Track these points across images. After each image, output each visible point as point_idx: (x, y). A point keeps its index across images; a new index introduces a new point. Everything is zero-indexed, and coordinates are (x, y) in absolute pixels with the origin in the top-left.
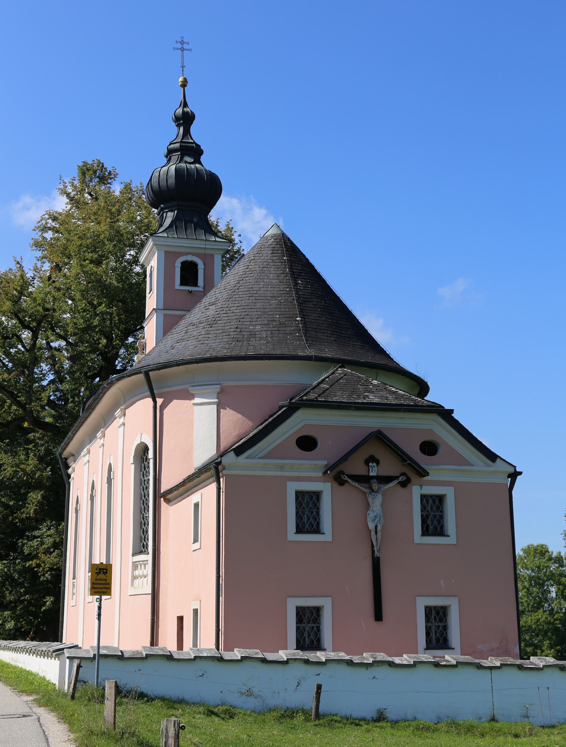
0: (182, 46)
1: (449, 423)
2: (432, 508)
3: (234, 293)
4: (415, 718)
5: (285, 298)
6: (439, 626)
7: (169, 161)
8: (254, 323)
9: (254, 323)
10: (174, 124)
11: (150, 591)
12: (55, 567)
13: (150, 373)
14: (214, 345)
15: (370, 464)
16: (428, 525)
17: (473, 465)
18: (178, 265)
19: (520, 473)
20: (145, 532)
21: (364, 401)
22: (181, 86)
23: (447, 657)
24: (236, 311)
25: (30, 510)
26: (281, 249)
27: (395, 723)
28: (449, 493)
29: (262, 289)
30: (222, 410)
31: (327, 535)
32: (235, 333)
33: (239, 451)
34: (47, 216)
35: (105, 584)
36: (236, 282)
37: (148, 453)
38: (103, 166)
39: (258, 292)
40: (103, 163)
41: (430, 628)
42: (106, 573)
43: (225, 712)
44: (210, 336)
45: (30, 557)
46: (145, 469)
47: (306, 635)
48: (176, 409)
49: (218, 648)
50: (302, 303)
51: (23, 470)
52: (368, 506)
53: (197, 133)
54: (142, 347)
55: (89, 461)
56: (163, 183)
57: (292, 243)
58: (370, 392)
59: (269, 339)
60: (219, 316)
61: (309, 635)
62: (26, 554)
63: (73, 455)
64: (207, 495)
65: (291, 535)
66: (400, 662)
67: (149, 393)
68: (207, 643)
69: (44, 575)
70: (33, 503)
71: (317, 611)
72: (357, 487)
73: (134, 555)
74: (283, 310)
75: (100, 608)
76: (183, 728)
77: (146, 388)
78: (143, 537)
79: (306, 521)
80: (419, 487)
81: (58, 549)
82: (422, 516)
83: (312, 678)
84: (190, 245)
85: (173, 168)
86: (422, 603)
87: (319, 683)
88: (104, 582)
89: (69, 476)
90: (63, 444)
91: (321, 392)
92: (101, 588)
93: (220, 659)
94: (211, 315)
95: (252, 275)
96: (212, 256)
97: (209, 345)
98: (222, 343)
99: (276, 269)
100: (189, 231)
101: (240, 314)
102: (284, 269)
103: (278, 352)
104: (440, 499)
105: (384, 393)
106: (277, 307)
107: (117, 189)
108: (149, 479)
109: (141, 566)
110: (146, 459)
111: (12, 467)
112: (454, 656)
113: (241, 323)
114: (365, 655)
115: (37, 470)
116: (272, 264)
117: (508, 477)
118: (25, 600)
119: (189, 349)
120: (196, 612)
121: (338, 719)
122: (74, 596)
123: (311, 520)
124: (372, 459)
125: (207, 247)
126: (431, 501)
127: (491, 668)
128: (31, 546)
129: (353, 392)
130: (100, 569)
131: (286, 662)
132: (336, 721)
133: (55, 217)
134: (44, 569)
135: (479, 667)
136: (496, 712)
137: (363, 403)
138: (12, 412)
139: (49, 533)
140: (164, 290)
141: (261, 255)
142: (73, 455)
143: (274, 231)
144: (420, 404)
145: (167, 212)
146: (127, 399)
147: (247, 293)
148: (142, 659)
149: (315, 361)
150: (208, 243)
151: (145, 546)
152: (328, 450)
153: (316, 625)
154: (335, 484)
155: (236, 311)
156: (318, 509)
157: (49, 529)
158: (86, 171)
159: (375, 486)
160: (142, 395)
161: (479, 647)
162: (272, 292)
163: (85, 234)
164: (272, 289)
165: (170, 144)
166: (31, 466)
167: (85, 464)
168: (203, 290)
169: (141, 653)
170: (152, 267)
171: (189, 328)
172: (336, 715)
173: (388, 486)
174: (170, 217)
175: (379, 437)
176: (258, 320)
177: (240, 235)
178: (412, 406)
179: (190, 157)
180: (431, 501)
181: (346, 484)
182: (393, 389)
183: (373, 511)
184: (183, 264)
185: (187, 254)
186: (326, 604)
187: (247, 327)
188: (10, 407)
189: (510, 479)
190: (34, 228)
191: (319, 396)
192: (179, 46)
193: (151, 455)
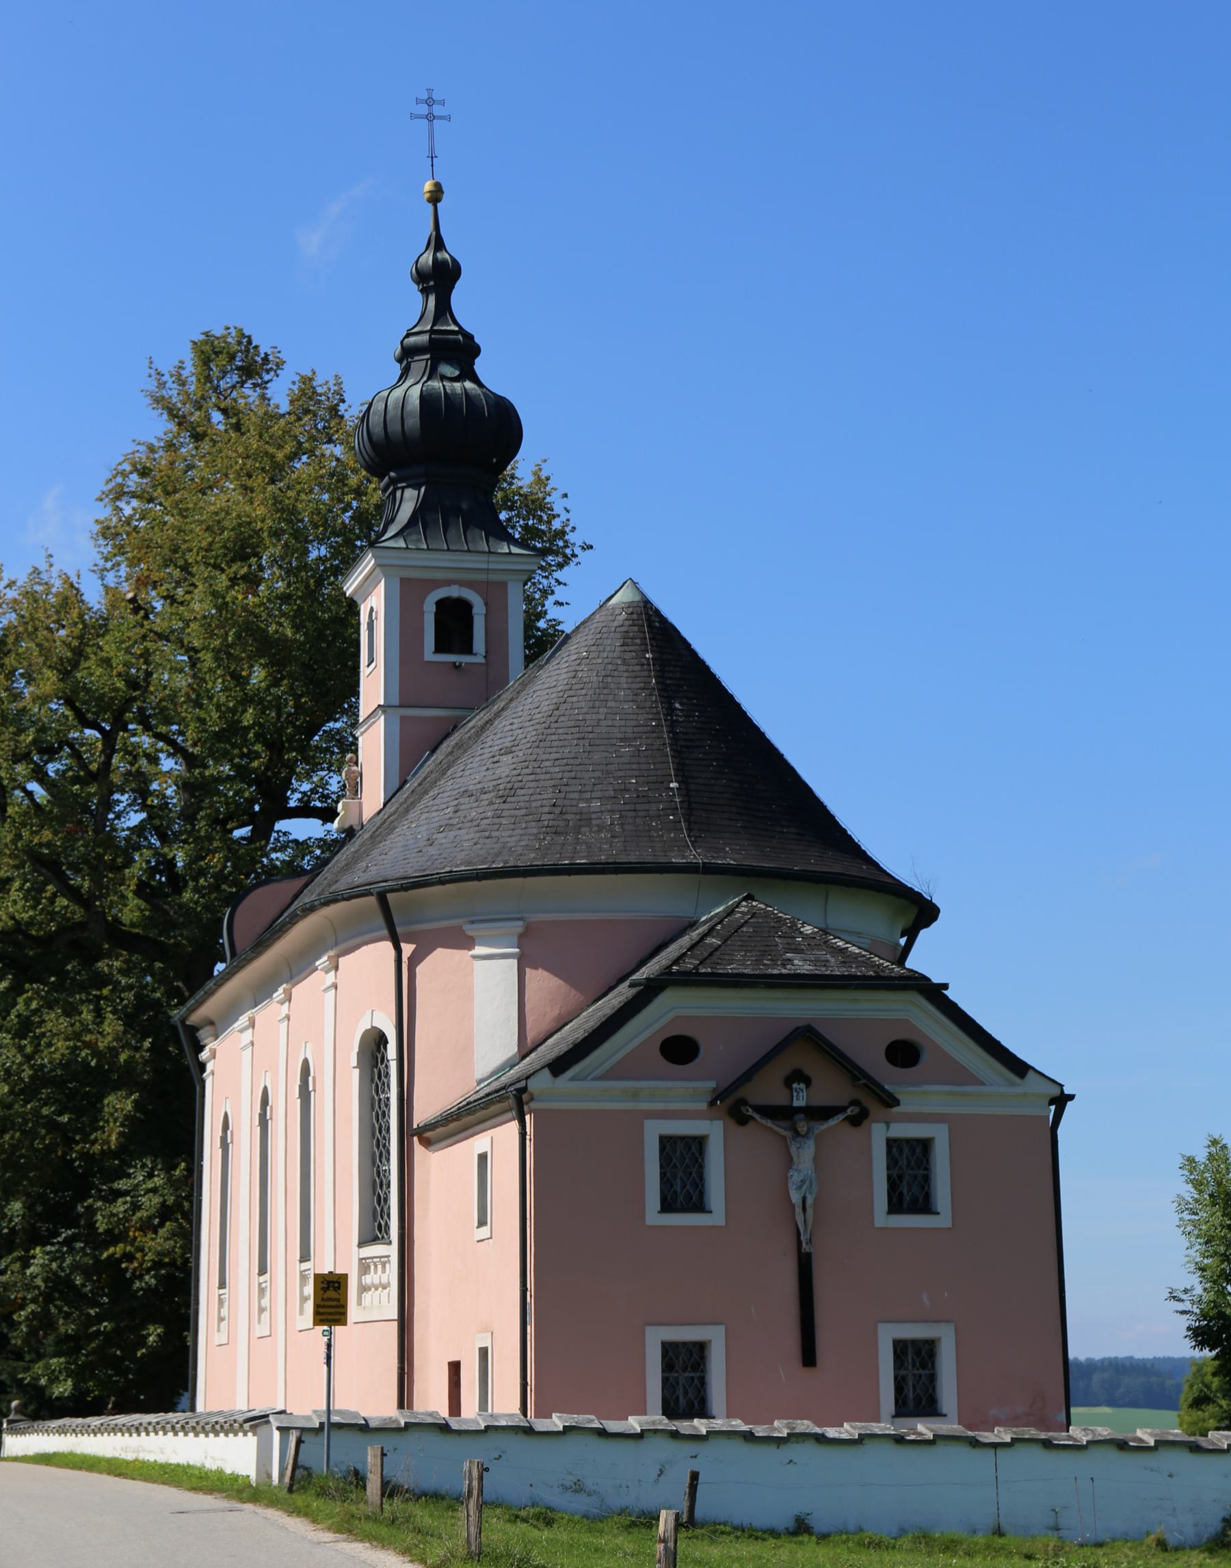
0: (430, 110)
1: (938, 1007)
2: (909, 1162)
3: (549, 731)
4: (861, 1530)
5: (649, 741)
6: (920, 1376)
7: (405, 373)
8: (588, 795)
9: (588, 795)
10: (415, 288)
11: (394, 1315)
12: (167, 1260)
13: (388, 895)
14: (512, 842)
15: (795, 1085)
16: (901, 1194)
17: (984, 1084)
18: (430, 608)
19: (1071, 1097)
20: (383, 1201)
21: (784, 971)
22: (429, 200)
23: (920, 1428)
24: (553, 770)
25: (109, 1136)
26: (641, 635)
27: (824, 1537)
28: (939, 1134)
29: (604, 723)
30: (527, 970)
31: (717, 1215)
32: (551, 816)
33: (558, 1066)
34: (127, 467)
35: (337, 1307)
36: (552, 707)
37: (385, 1048)
38: (250, 342)
39: (597, 730)
40: (249, 337)
41: (904, 1378)
42: (339, 1288)
43: (538, 1517)
44: (504, 821)
45: (113, 1237)
46: (380, 1078)
47: (680, 1391)
48: (440, 965)
49: (525, 1415)
50: (682, 750)
51: (87, 1045)
52: (789, 1162)
53: (467, 305)
54: (353, 783)
55: (252, 1043)
56: (395, 427)
57: (663, 620)
58: (797, 951)
59: (617, 828)
60: (520, 778)
61: (686, 1393)
62: (101, 1230)
63: (212, 1023)
64: (502, 1141)
65: (653, 1214)
66: (837, 1435)
67: (385, 932)
68: (506, 1403)
69: (141, 1277)
70: (115, 1120)
71: (699, 1351)
72: (770, 1128)
73: (362, 1244)
74: (644, 767)
75: (329, 1346)
76: (487, 1470)
77: (380, 920)
78: (379, 1209)
79: (679, 1190)
80: (883, 1126)
81: (170, 1220)
82: (889, 1177)
83: (682, 1460)
84: (456, 564)
85: (416, 392)
86: (887, 1335)
87: (696, 1469)
88: (334, 1303)
89: (202, 1067)
90: (192, 1002)
91: (706, 954)
92: (330, 1314)
93: (529, 1431)
94: (504, 775)
95: (584, 692)
96: (503, 586)
97: (502, 840)
98: (526, 838)
99: (630, 680)
100: (452, 532)
101: (560, 775)
102: (647, 680)
103: (633, 858)
104: (925, 1145)
105: (822, 954)
106: (633, 760)
107: (280, 392)
108: (388, 1099)
109: (376, 1266)
110: (382, 1061)
111: (67, 1039)
112: (933, 1426)
113: (562, 795)
114: (776, 1423)
115: (123, 1047)
116: (622, 668)
117: (1051, 1103)
118: (98, 1332)
119: (462, 848)
120: (484, 1353)
121: (728, 1529)
122: (224, 1324)
123: (688, 1187)
124: (798, 1076)
125: (491, 566)
126: (906, 1150)
127: (995, 1446)
128: (113, 1215)
129: (764, 953)
130: (329, 1283)
131: (640, 1436)
132: (723, 1533)
133: (145, 468)
134: (141, 1265)
135: (975, 1443)
136: (1003, 1524)
137: (781, 976)
138: (57, 913)
139: (150, 1185)
140: (401, 663)
141: (601, 648)
142: (212, 1023)
143: (624, 596)
144: (887, 973)
145: (403, 489)
146: (345, 940)
147: (574, 730)
148: (398, 1430)
149: (704, 873)
150: (493, 558)
151: (384, 1229)
152: (719, 1059)
153: (698, 1374)
154: (732, 1123)
155: (553, 770)
156: (701, 1167)
157: (150, 1176)
158: (210, 352)
159: (802, 1127)
160: (374, 935)
161: (992, 1412)
162: (623, 729)
163: (219, 522)
164: (623, 723)
165: (408, 336)
166: (110, 1038)
167: (244, 1048)
168: (483, 661)
169: (396, 1421)
170: (372, 609)
171: (462, 800)
172: (725, 1524)
173: (825, 1126)
174: (409, 500)
175: (807, 1036)
176: (596, 788)
177: (565, 496)
178: (870, 978)
179: (452, 365)
180: (906, 1150)
181: (751, 1123)
182: (841, 944)
183: (799, 1171)
184: (441, 604)
185: (449, 583)
186: (715, 1337)
187: (574, 803)
188: (52, 900)
189: (1053, 1108)
190: (98, 494)
191: (701, 963)
192: (424, 109)
193: (391, 1051)
